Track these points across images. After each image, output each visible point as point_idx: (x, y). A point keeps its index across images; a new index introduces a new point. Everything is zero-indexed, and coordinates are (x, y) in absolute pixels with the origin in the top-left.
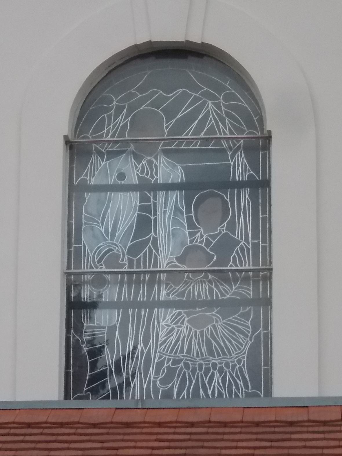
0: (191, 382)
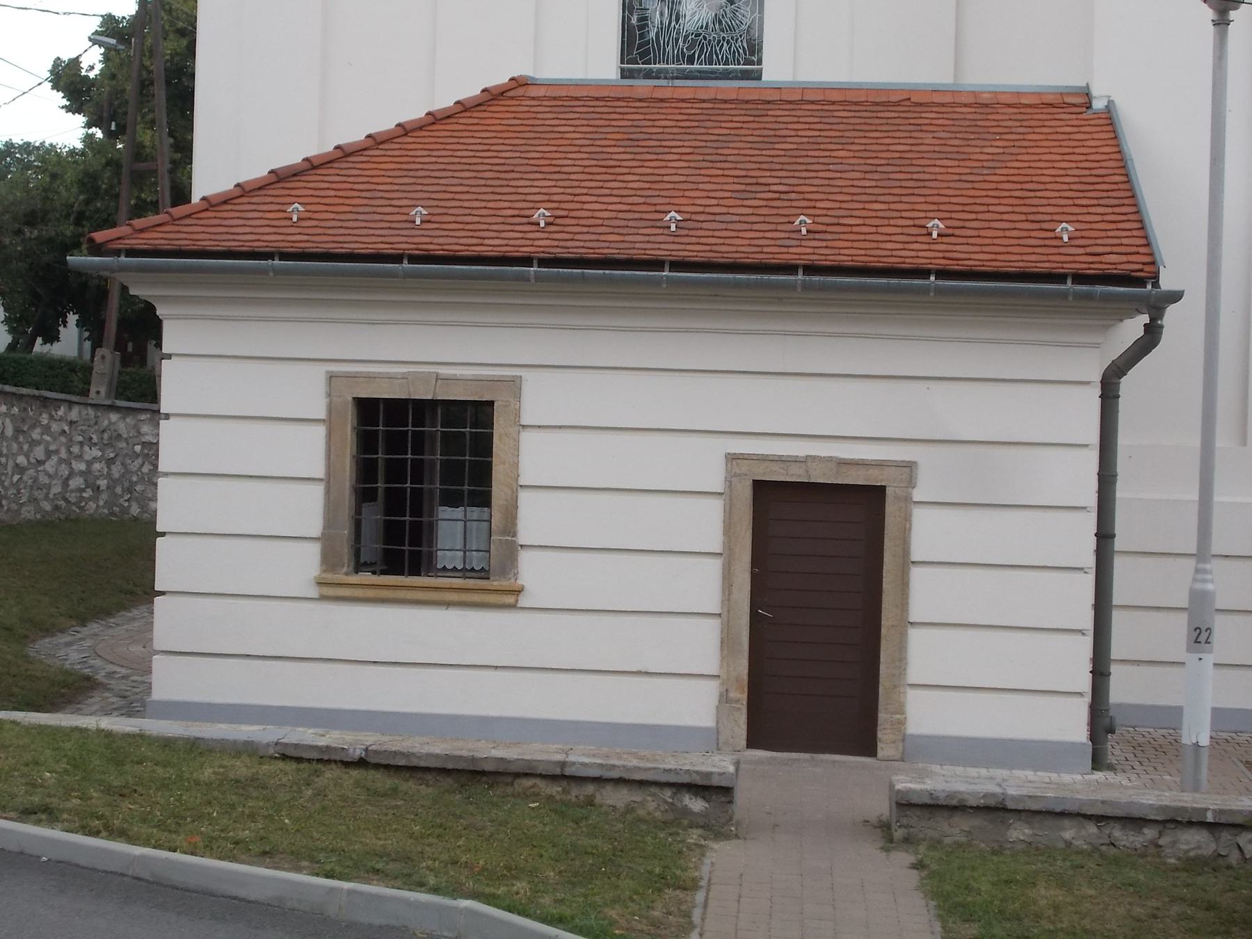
0: (707, 49)
